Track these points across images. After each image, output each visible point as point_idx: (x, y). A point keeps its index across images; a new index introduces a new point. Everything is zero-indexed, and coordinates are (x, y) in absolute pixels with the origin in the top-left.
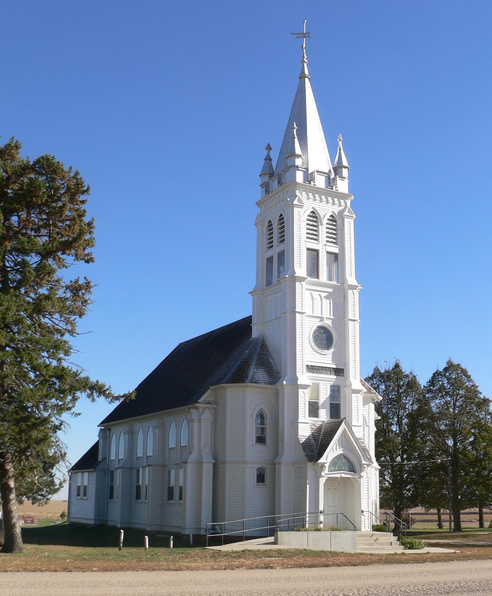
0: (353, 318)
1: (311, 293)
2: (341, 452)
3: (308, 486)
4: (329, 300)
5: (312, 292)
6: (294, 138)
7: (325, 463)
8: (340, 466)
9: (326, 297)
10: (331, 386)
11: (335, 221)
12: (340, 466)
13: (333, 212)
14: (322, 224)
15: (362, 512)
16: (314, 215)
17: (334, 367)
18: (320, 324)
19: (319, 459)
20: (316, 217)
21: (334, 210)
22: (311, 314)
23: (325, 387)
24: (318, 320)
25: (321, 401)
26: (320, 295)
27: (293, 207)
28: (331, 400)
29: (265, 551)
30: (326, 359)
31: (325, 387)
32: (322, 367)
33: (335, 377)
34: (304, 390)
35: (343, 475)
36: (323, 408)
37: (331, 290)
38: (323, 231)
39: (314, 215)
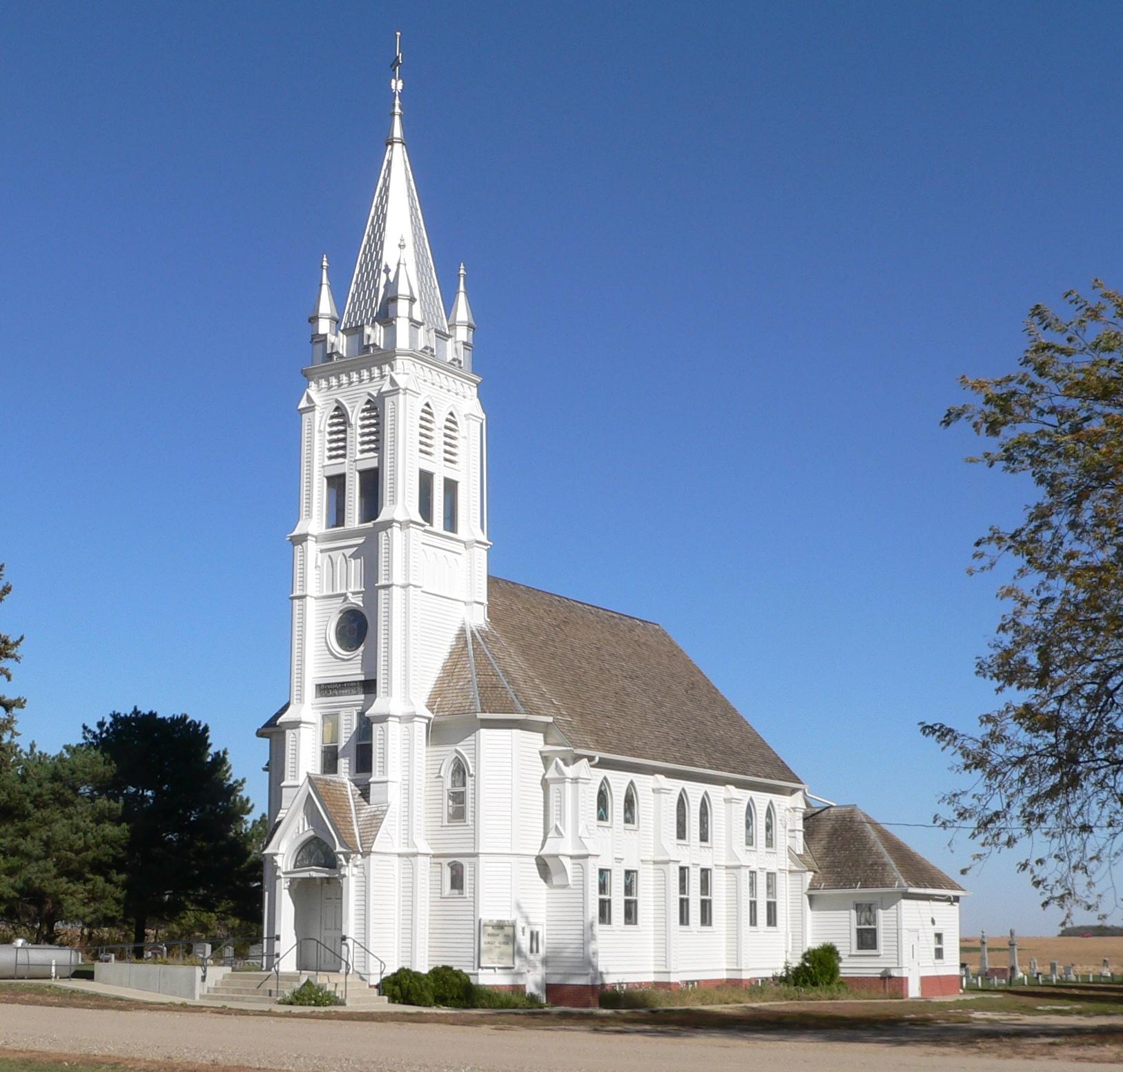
2: (312, 833)
7: (276, 854)
11: (374, 409)
13: (369, 394)
14: (350, 425)
15: (344, 938)
16: (340, 412)
17: (362, 678)
21: (370, 390)
33: (362, 697)
35: (314, 874)
37: (360, 541)
39: (340, 412)
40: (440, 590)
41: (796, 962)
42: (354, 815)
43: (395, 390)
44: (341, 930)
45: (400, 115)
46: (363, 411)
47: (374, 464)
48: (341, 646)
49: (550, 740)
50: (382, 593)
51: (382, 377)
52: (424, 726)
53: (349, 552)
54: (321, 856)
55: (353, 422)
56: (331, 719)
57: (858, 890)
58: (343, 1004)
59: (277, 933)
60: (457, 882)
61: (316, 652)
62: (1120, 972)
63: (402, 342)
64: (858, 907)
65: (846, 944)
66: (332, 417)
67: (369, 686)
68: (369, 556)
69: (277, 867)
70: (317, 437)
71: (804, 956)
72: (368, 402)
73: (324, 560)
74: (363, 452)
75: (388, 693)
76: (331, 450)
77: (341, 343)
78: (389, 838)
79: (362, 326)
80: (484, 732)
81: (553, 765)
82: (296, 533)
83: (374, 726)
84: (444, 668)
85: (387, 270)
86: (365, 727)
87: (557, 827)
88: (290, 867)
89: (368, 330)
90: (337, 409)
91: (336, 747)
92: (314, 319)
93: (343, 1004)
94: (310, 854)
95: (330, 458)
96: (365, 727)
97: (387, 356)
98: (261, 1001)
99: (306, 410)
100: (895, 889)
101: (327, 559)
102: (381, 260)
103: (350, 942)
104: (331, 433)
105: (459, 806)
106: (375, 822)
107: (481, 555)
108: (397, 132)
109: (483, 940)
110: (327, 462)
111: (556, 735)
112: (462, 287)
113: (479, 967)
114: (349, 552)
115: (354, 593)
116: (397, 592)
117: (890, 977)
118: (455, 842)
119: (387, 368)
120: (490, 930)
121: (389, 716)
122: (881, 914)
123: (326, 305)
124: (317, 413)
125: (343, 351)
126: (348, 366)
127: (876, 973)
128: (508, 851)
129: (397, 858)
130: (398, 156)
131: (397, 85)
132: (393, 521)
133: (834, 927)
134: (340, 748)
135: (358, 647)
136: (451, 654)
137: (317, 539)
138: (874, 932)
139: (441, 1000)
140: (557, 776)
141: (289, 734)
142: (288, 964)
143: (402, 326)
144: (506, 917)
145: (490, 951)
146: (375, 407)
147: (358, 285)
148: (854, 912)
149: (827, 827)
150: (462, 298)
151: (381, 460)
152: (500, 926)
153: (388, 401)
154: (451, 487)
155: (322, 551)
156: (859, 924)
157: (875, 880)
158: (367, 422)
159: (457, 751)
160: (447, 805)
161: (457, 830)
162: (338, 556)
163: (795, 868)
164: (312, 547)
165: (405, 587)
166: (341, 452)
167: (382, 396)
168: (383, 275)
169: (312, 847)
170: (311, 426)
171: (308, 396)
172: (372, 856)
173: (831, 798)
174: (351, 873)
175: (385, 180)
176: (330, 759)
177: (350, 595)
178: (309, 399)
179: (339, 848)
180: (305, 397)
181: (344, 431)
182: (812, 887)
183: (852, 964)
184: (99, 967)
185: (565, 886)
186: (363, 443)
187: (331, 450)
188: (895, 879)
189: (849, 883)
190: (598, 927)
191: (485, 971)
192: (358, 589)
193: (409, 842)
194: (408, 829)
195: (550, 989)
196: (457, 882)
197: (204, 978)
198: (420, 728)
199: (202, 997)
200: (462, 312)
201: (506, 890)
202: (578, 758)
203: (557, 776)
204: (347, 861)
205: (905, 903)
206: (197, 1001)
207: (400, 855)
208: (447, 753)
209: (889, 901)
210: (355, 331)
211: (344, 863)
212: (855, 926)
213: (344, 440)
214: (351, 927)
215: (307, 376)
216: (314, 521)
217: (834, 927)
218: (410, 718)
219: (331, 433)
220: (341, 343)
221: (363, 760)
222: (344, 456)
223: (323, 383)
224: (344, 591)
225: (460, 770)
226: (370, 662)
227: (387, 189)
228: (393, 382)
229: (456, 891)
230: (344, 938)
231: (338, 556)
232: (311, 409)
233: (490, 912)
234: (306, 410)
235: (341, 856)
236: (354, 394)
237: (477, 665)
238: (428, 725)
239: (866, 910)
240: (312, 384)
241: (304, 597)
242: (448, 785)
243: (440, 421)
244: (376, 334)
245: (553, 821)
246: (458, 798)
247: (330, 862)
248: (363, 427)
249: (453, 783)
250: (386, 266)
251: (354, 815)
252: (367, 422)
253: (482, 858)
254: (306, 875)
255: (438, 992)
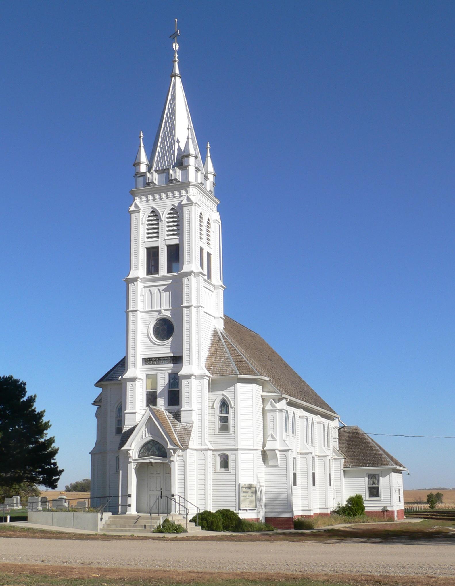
0: (187, 304)
1: (149, 290)
2: (151, 438)
3: (121, 471)
4: (168, 292)
5: (150, 288)
6: (140, 146)
7: (129, 450)
8: (153, 451)
9: (165, 290)
10: (169, 374)
11: (177, 213)
12: (153, 451)
13: (173, 205)
14: (161, 221)
15: (173, 495)
16: (155, 214)
17: (172, 355)
18: (159, 316)
19: (122, 447)
20: (156, 216)
21: (173, 203)
22: (150, 309)
23: (163, 376)
24: (157, 313)
25: (159, 389)
26: (158, 289)
27: (183, 207)
28: (169, 388)
29: (29, 529)
30: (165, 349)
31: (163, 376)
32: (160, 358)
33: (172, 365)
34: (132, 383)
35: (153, 461)
36: (160, 397)
37: (169, 282)
38: (164, 227)
39: (155, 214)
40: (206, 310)
41: (344, 503)
42: (172, 428)
43: (190, 203)
44: (171, 491)
45: (178, 62)
46: (169, 214)
47: (176, 242)
48: (157, 338)
49: (265, 390)
50: (185, 310)
51: (181, 196)
52: (207, 381)
53: (161, 288)
54: (155, 450)
55: (163, 219)
56: (152, 378)
57: (370, 468)
58: (186, 532)
59: (129, 493)
60: (225, 463)
61: (143, 342)
62: (453, 505)
63: (192, 178)
64: (369, 476)
65: (365, 494)
66: (149, 216)
67: (177, 359)
68: (176, 291)
69: (130, 457)
70: (141, 226)
71: (347, 501)
72: (172, 209)
73: (146, 291)
74: (168, 235)
75: (190, 363)
76: (148, 234)
77: (155, 178)
78: (194, 443)
79: (168, 169)
80: (239, 384)
81: (270, 403)
82: (130, 276)
83: (128, 383)
84: (210, 351)
85: (178, 142)
86: (175, 381)
87: (272, 435)
88: (137, 458)
89: (171, 172)
90: (152, 212)
91: (155, 392)
92: (137, 164)
93: (186, 532)
94: (148, 450)
95: (148, 238)
96: (175, 381)
97: (185, 185)
98: (140, 531)
99: (134, 212)
100: (390, 467)
101: (148, 292)
102: (174, 135)
103: (177, 497)
104: (148, 225)
105: (224, 423)
106: (186, 433)
107: (221, 292)
108: (177, 71)
109: (242, 494)
110: (147, 240)
111: (270, 387)
112: (209, 155)
113: (240, 509)
114: (161, 288)
115: (165, 310)
116: (193, 309)
117: (387, 511)
118: (223, 442)
119: (183, 192)
120: (244, 490)
121: (136, 378)
122: (381, 479)
123: (143, 158)
124: (141, 214)
125: (156, 182)
126: (159, 190)
127: (379, 509)
128: (252, 448)
129: (195, 452)
130: (178, 82)
131: (176, 46)
132: (192, 272)
133: (359, 486)
134: (158, 392)
135: (168, 339)
136: (212, 344)
137: (142, 281)
138: (378, 488)
139: (226, 528)
140: (272, 408)
141: (129, 385)
142: (132, 511)
143: (191, 170)
144: (254, 483)
145: (244, 500)
146: (177, 213)
147: (161, 148)
148: (367, 479)
149: (346, 436)
150: (209, 160)
151: (181, 240)
152: (250, 487)
153: (185, 209)
154: (209, 255)
155: (144, 287)
156: (370, 484)
157: (378, 463)
158: (171, 220)
159: (223, 395)
160: (217, 424)
161: (224, 436)
162: (155, 290)
163: (336, 457)
164: (139, 285)
165: (197, 307)
166: (155, 235)
167: (181, 206)
168: (176, 144)
169: (150, 446)
170: (137, 220)
171: (135, 203)
172: (188, 451)
173: (350, 424)
174: (176, 460)
175: (172, 95)
176: (151, 399)
177: (163, 311)
178: (136, 206)
179: (170, 446)
180: (133, 205)
181: (158, 224)
182: (345, 466)
183: (371, 505)
184: (31, 515)
185: (275, 466)
186: (168, 231)
187: (148, 234)
188: (389, 462)
189: (365, 464)
190: (293, 487)
191: (242, 511)
192: (168, 308)
193: (202, 442)
194: (202, 437)
195: (267, 520)
196: (225, 463)
197: (101, 519)
198: (206, 381)
199: (101, 530)
200: (210, 168)
201: (249, 469)
202: (280, 399)
203: (272, 408)
204: (175, 453)
205: (393, 474)
206: (99, 532)
207: (197, 450)
208: (218, 396)
209: (385, 473)
210: (163, 171)
211: (173, 454)
212: (367, 486)
213: (158, 228)
214: (176, 489)
215: (133, 194)
216: (139, 269)
217: (359, 486)
218: (202, 377)
219: (148, 225)
220: (155, 178)
221: (174, 398)
222: (157, 237)
223: (144, 198)
224: (159, 309)
225: (225, 405)
226: (178, 346)
227: (174, 99)
228: (188, 199)
229: (224, 469)
230: (173, 495)
231: (155, 290)
232: (137, 211)
233: (244, 480)
234: (134, 212)
235: (172, 451)
236: (164, 205)
237: (230, 350)
238: (209, 381)
239: (373, 478)
240: (137, 198)
241: (136, 311)
242: (218, 412)
243: (205, 221)
244: (178, 174)
245: (269, 432)
246: (224, 420)
247: (163, 453)
248: (168, 222)
249: (221, 412)
250: (178, 139)
251: (172, 428)
252: (171, 220)
253: (239, 452)
254: (148, 461)
255: (221, 522)
